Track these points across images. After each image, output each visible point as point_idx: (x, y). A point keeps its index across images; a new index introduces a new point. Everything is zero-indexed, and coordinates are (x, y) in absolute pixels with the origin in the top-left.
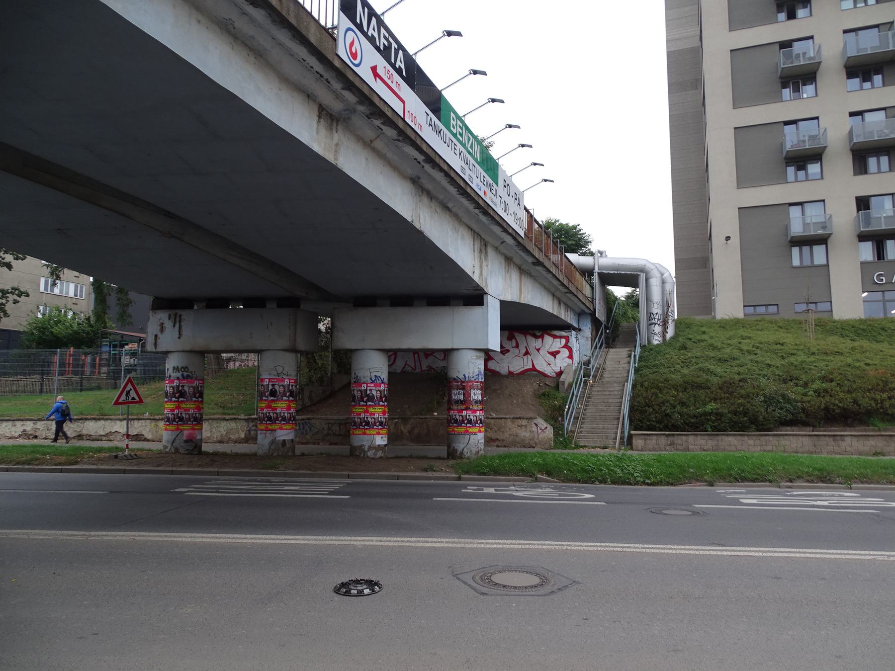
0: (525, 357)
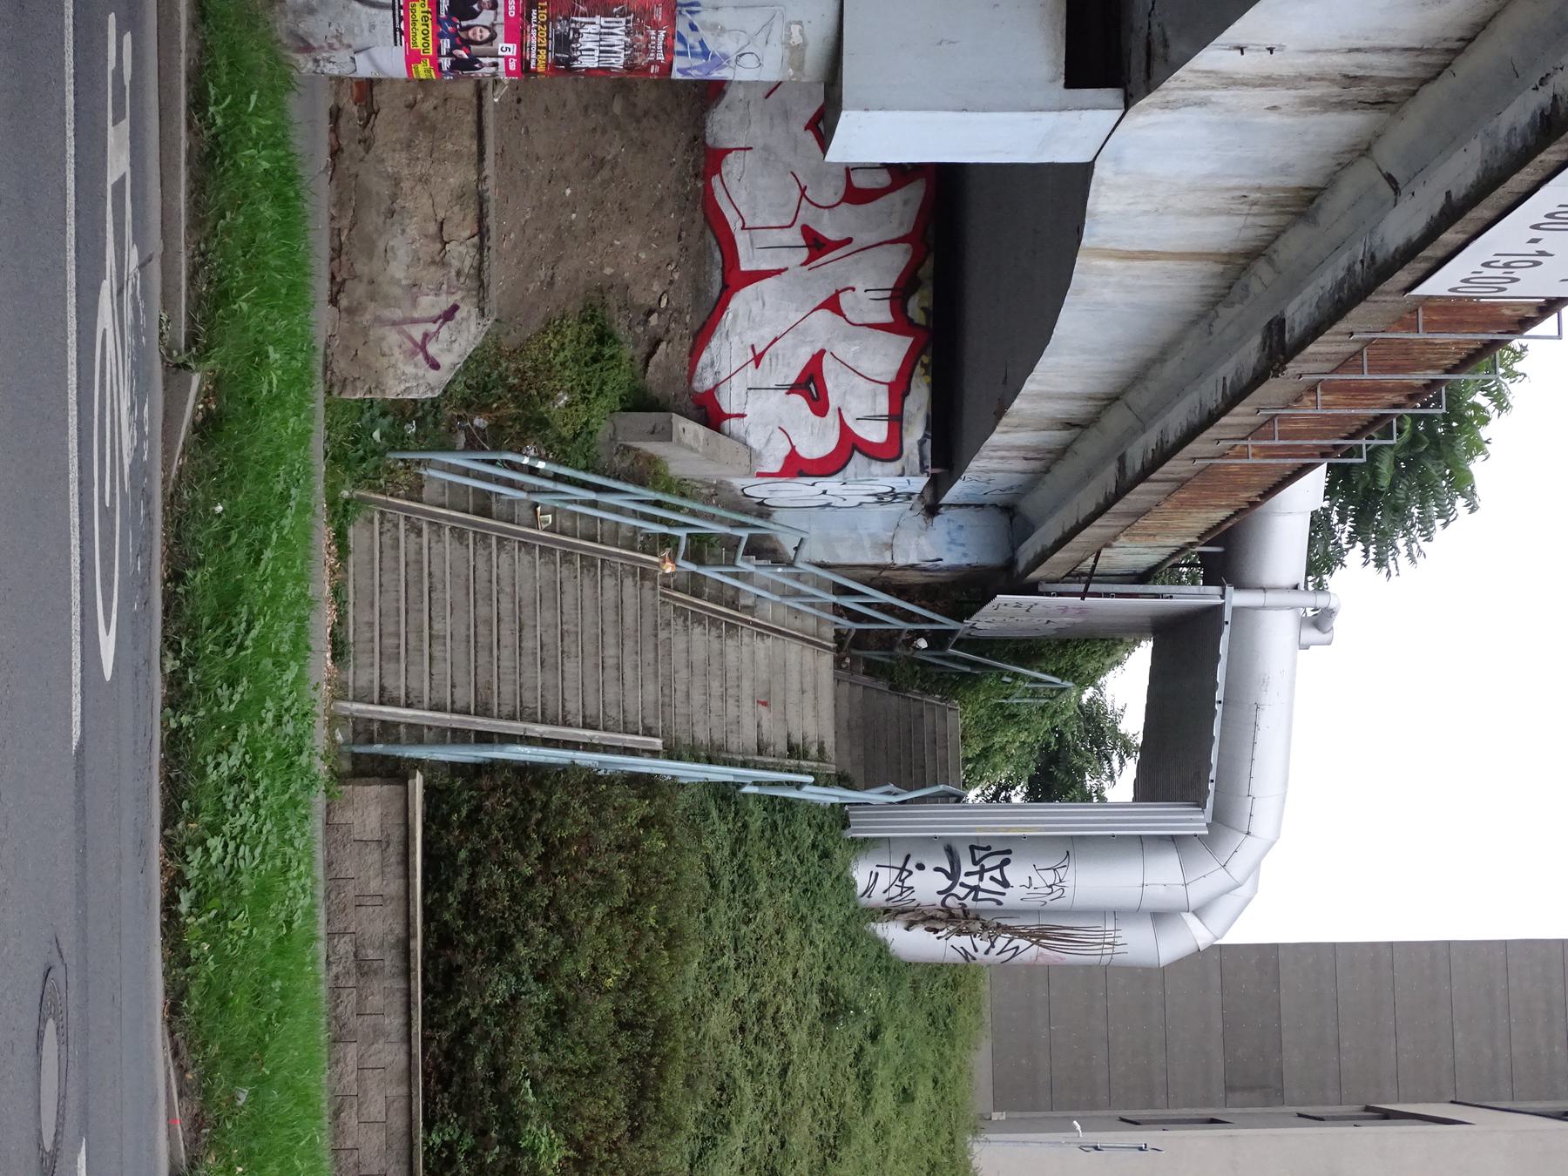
0: (794, 236)
